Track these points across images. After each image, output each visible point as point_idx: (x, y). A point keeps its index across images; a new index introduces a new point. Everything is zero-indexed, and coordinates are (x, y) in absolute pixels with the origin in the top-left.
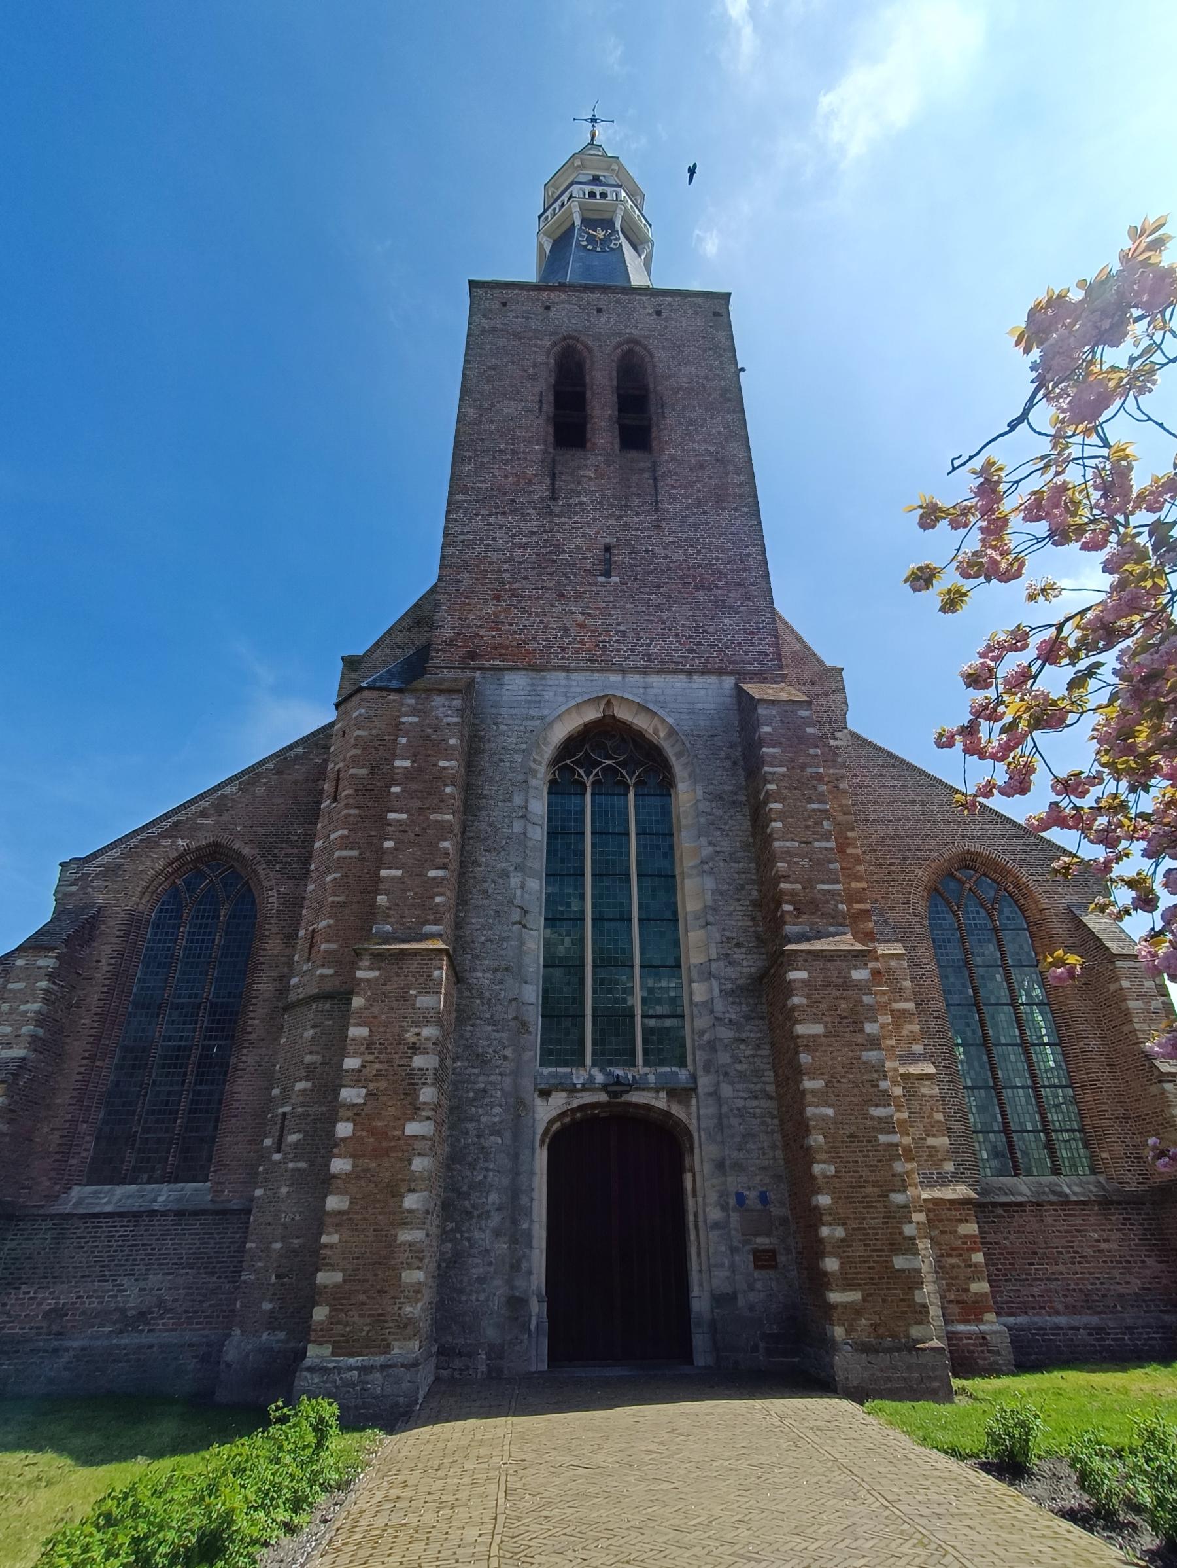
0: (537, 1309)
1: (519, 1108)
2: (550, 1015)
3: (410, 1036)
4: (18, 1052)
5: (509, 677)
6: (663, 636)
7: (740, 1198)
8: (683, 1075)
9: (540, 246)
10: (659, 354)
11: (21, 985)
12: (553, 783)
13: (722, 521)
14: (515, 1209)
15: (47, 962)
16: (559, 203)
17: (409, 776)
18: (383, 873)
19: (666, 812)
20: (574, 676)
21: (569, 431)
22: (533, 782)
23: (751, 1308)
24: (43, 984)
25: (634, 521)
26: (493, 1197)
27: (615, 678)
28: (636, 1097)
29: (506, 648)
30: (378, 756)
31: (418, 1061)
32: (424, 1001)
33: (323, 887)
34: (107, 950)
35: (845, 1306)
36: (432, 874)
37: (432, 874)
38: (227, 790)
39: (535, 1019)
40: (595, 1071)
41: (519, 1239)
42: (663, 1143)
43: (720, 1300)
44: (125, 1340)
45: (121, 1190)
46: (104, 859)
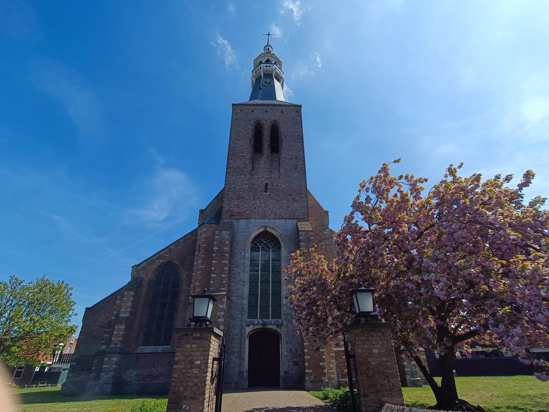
0: (246, 374)
1: (242, 329)
2: (250, 306)
3: (218, 314)
4: (127, 315)
5: (241, 221)
6: (280, 209)
7: (291, 350)
8: (280, 321)
9: (252, 80)
10: (282, 125)
11: (126, 299)
12: (252, 248)
13: (296, 175)
14: (241, 352)
15: (132, 293)
16: (259, 67)
17: (218, 251)
18: (212, 275)
19: (279, 255)
20: (257, 220)
21: (257, 148)
22: (246, 249)
23: (292, 374)
24: (132, 298)
25: (273, 176)
26: (236, 349)
27: (267, 221)
28: (269, 327)
29: (241, 213)
30: (210, 240)
31: (220, 320)
32: (221, 306)
33: (197, 274)
34: (144, 289)
35: (309, 373)
36: (222, 276)
37: (222, 276)
38: (172, 247)
39: (246, 308)
40: (260, 320)
41: (242, 359)
42: (275, 337)
43: (286, 372)
44: (153, 382)
45: (150, 347)
46: (142, 265)
